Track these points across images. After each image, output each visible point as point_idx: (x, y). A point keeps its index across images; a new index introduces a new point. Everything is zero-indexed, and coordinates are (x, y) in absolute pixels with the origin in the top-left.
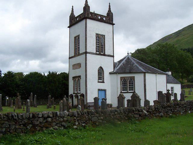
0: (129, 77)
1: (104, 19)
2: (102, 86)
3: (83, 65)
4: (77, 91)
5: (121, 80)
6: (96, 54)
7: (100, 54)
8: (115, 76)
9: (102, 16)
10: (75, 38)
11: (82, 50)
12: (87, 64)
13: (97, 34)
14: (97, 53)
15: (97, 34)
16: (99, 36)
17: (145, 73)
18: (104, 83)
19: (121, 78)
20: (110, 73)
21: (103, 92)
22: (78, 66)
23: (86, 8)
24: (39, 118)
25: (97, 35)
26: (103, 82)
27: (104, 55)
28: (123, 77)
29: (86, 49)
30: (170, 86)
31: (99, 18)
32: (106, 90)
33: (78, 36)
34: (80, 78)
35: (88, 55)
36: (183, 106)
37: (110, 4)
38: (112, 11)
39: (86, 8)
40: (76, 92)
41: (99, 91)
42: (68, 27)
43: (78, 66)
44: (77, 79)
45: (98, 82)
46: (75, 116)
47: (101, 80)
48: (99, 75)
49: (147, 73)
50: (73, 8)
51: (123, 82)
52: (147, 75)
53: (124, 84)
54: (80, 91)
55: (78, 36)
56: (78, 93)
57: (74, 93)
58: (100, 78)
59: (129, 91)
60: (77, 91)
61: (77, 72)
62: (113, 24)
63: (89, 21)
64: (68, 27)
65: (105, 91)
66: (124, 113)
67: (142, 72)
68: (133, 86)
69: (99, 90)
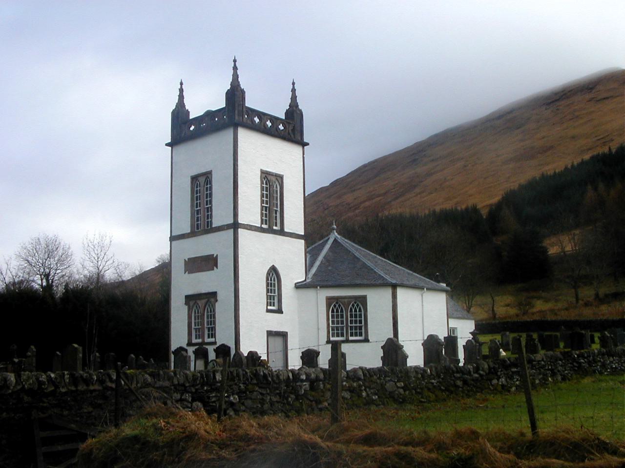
0: (350, 297)
1: (281, 127)
2: (276, 323)
3: (225, 262)
4: (200, 335)
5: (328, 305)
6: (261, 230)
7: (270, 231)
8: (310, 294)
9: (265, 114)
10: (194, 179)
11: (220, 216)
12: (240, 259)
13: (263, 172)
14: (264, 226)
15: (263, 172)
16: (278, 178)
17: (394, 287)
18: (282, 313)
19: (330, 301)
20: (299, 286)
21: (279, 341)
22: (208, 262)
23: (235, 94)
24: (302, 381)
25: (264, 175)
26: (280, 311)
27: (282, 232)
28: (337, 299)
29: (236, 215)
30: (453, 323)
31: (257, 120)
32: (287, 333)
33: (207, 176)
34: (212, 300)
35: (241, 231)
36: (540, 365)
37: (235, 61)
38: (243, 84)
39: (235, 94)
40: (200, 341)
41: (271, 339)
42: (167, 145)
43: (208, 262)
44: (201, 303)
45: (268, 311)
46: (359, 379)
47: (274, 306)
48: (268, 291)
49: (403, 286)
50: (181, 87)
51: (333, 311)
52: (400, 292)
53: (356, 316)
54: (213, 335)
55: (207, 176)
56: (203, 343)
57: (190, 344)
58: (270, 300)
59: (351, 338)
60: (200, 335)
61: (203, 282)
62: (304, 144)
63: (242, 133)
64: (167, 145)
65: (283, 335)
66: (437, 375)
67: (384, 284)
68: (360, 322)
69: (270, 334)
